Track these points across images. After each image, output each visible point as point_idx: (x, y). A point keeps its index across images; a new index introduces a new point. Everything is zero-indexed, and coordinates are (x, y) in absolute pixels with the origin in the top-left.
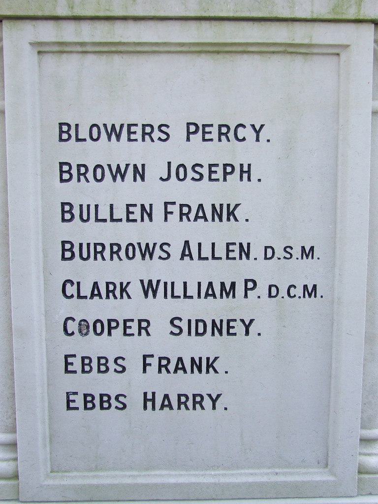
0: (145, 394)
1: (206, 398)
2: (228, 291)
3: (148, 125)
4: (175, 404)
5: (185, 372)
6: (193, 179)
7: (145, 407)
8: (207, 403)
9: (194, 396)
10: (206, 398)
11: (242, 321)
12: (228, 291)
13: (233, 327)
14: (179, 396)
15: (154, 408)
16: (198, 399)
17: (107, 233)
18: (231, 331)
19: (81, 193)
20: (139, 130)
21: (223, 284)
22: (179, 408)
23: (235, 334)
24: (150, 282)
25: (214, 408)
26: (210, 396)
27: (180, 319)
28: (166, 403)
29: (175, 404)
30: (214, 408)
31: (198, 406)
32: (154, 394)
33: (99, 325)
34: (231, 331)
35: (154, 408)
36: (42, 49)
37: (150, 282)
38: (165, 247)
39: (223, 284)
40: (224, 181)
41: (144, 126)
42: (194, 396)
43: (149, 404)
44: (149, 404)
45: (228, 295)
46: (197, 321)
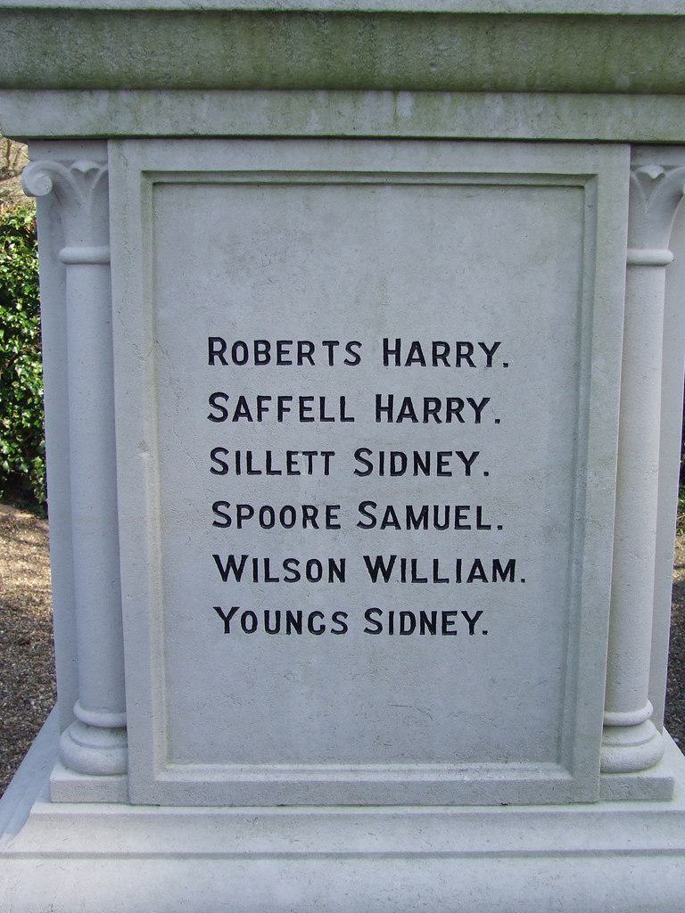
0: (379, 397)
1: (477, 349)
2: (417, 519)
3: (306, 342)
4: (428, 357)
5: (415, 420)
6: (228, 505)
7: (386, 362)
8: (479, 356)
9: (449, 401)
10: (477, 349)
11: (461, 454)
12: (417, 519)
13: (447, 463)
14: (427, 401)
15: (398, 363)
16: (465, 350)
17: (278, 491)
18: (444, 469)
19: (250, 540)
20: (293, 349)
21: (409, 509)
22: (426, 420)
23: (449, 474)
24: (379, 559)
25: (478, 419)
26: (482, 345)
27: (374, 505)
28: (390, 519)
29: (428, 357)
30: (478, 419)
31: (464, 361)
32: (398, 341)
33: (288, 514)
34: (444, 469)
35: (398, 363)
36: (157, 180)
37: (379, 559)
38: (354, 348)
39: (409, 509)
40: (383, 453)
41: (300, 344)
42: (459, 345)
43: (392, 358)
44: (392, 358)
45: (417, 525)
46: (393, 455)
